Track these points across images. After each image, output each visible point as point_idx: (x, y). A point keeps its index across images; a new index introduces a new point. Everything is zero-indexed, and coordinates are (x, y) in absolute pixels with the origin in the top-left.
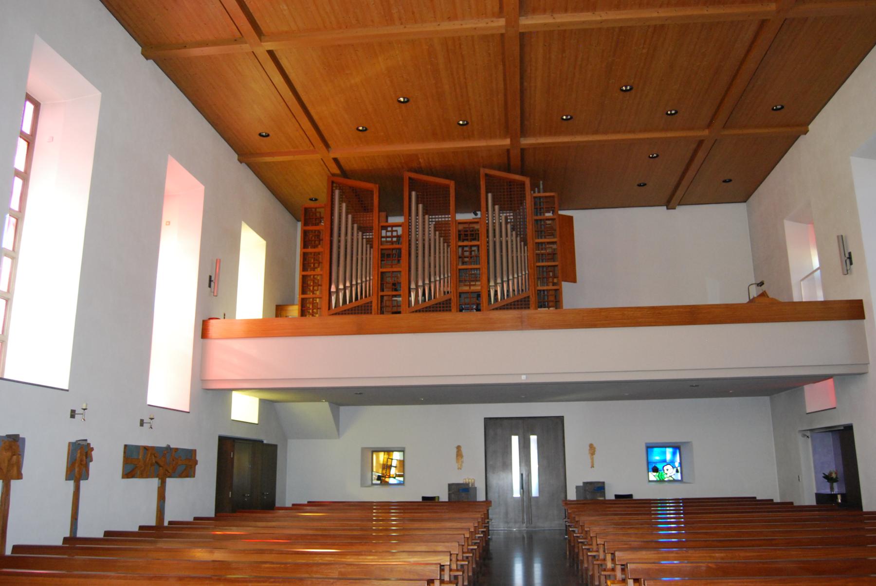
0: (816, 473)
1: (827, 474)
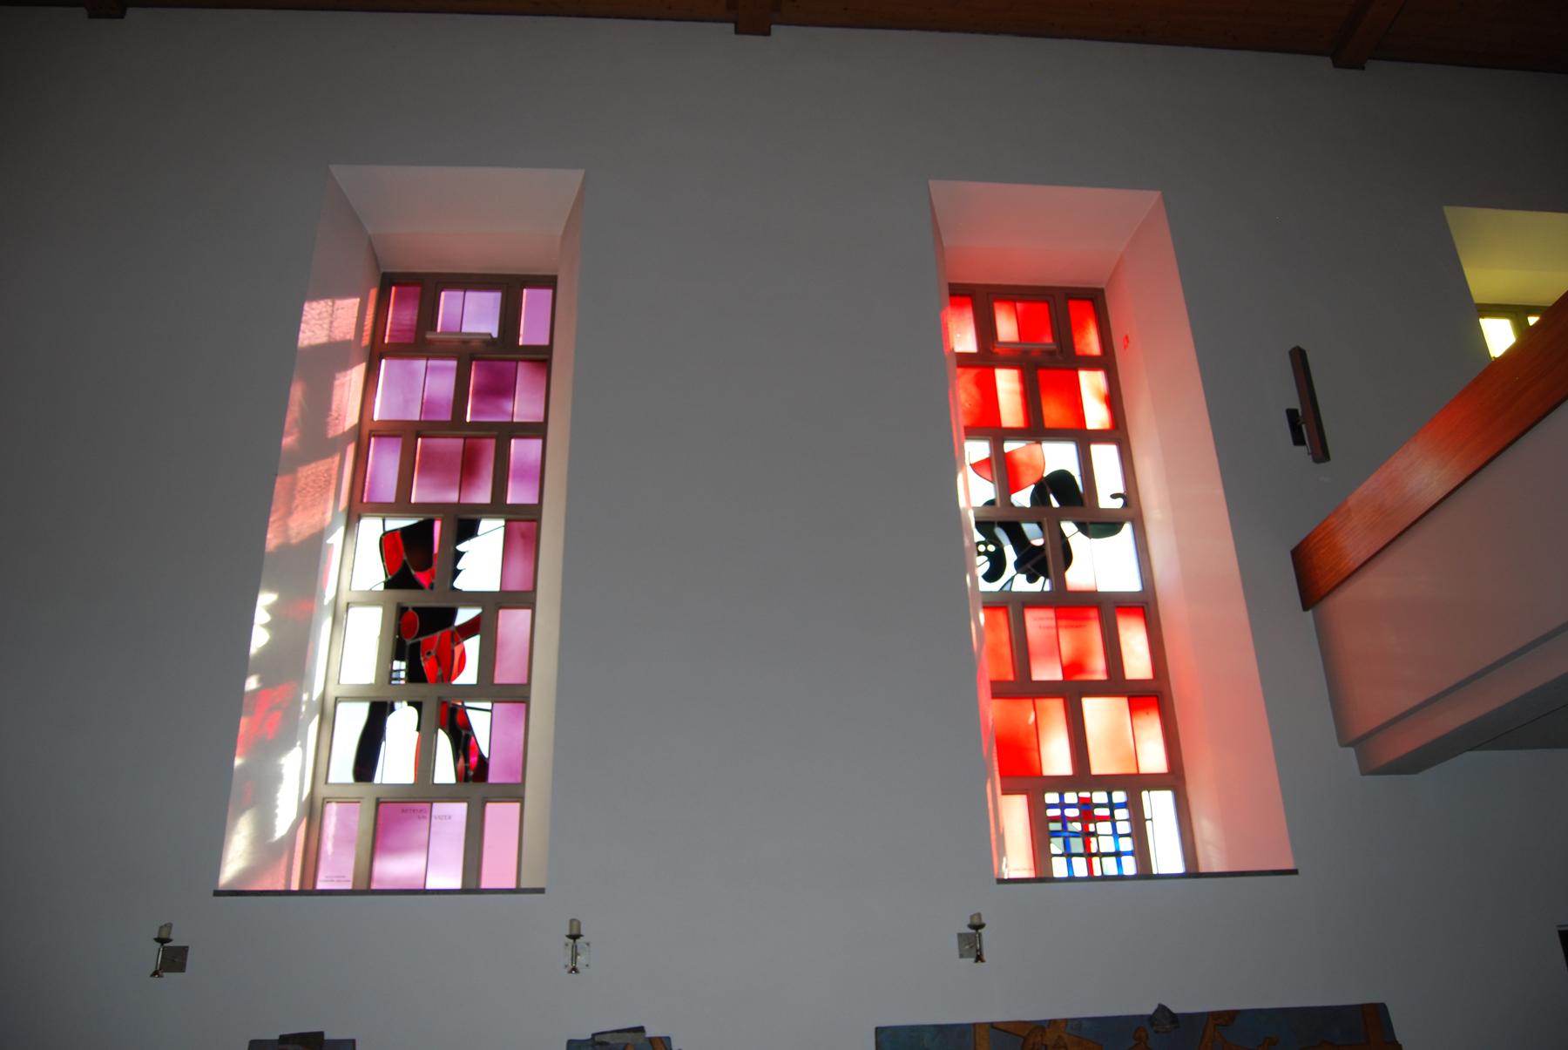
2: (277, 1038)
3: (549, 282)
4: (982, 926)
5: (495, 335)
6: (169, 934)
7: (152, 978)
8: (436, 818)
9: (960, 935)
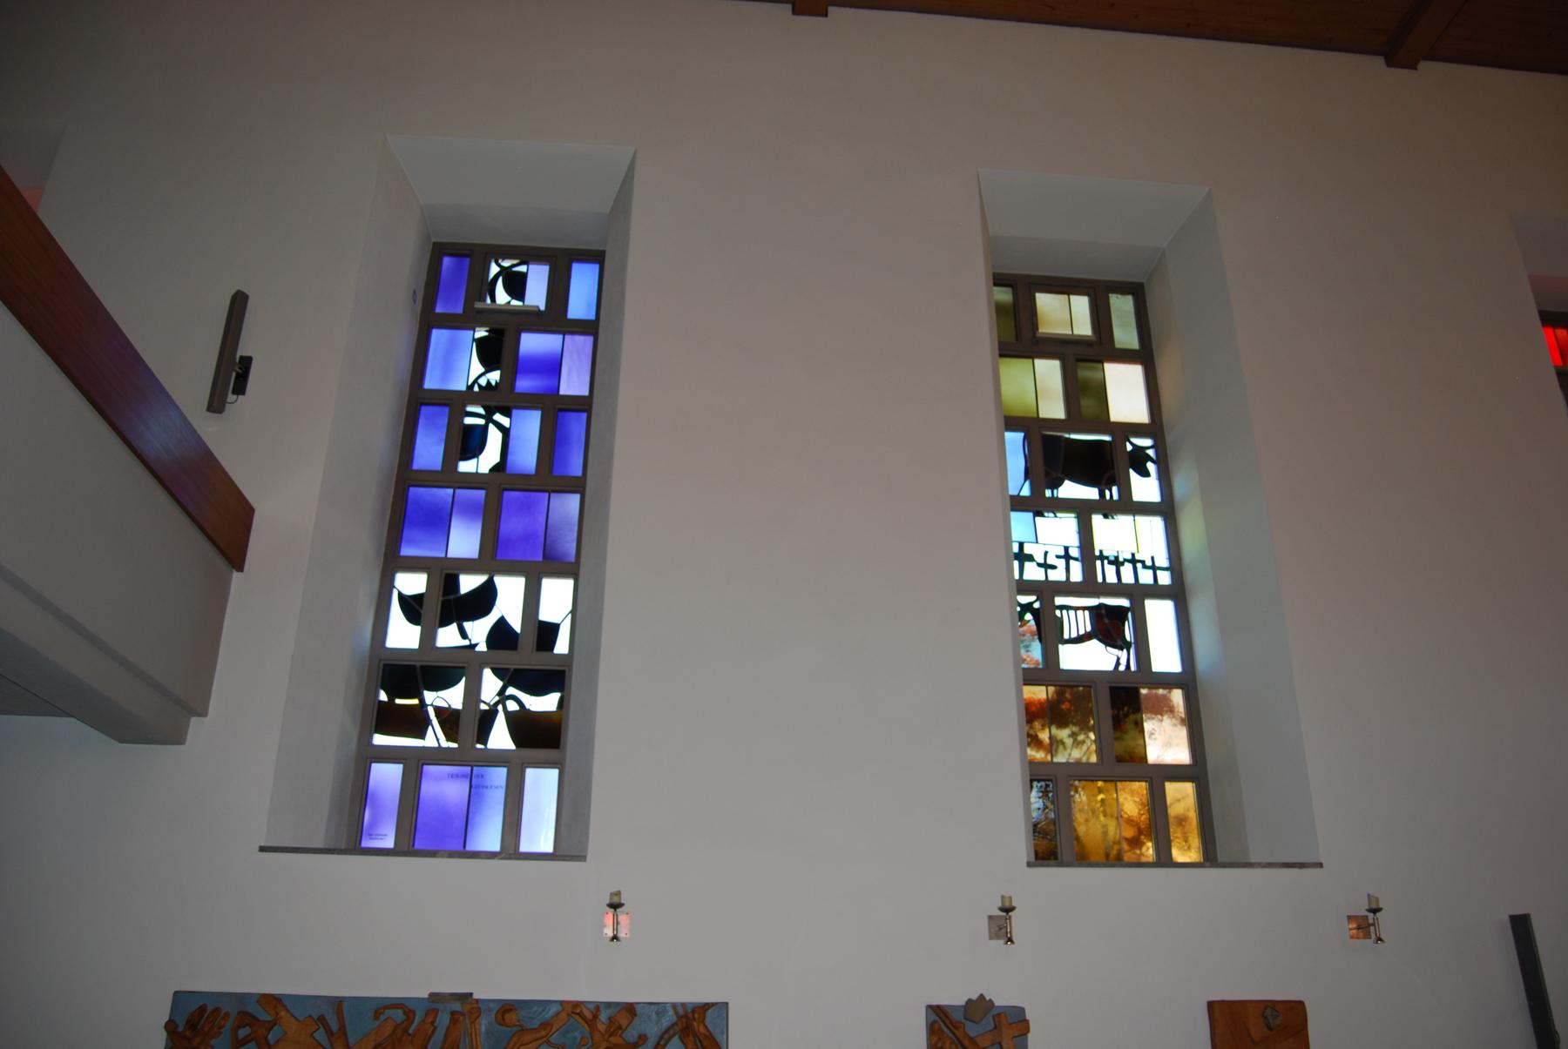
2: (426, 996)
3: (596, 257)
4: (1012, 909)
5: (542, 308)
6: (620, 899)
7: (612, 943)
8: (501, 787)
9: (990, 917)
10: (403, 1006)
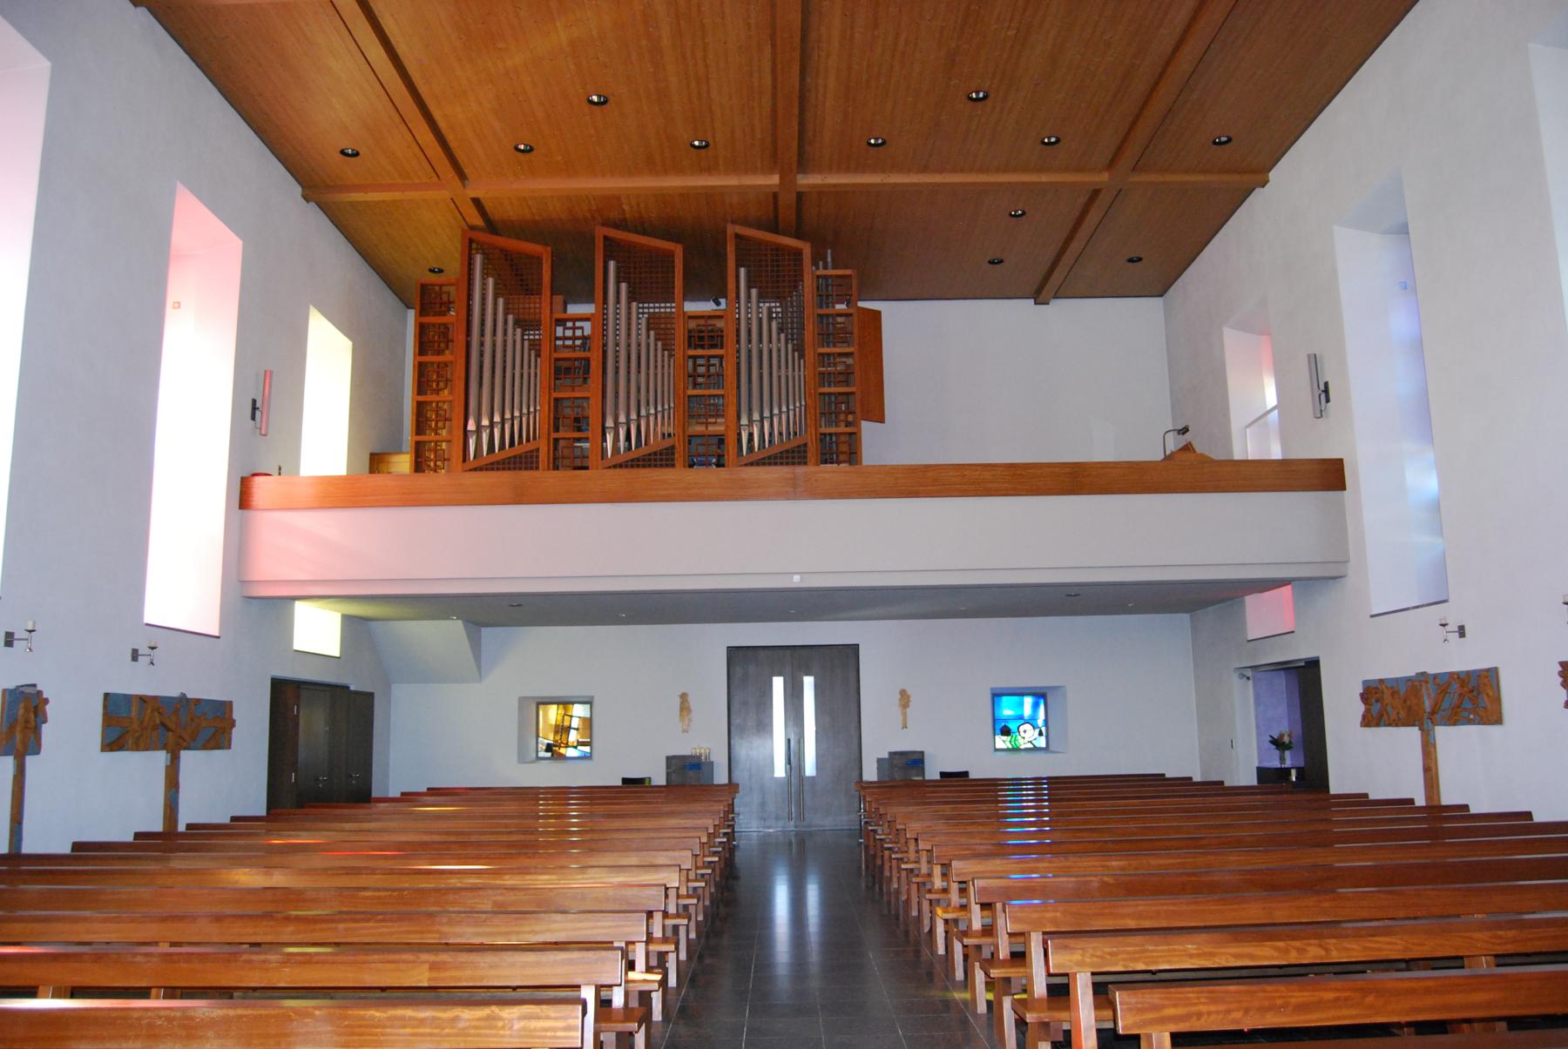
0: (1259, 734)
1: (1276, 737)
10: (1408, 679)
